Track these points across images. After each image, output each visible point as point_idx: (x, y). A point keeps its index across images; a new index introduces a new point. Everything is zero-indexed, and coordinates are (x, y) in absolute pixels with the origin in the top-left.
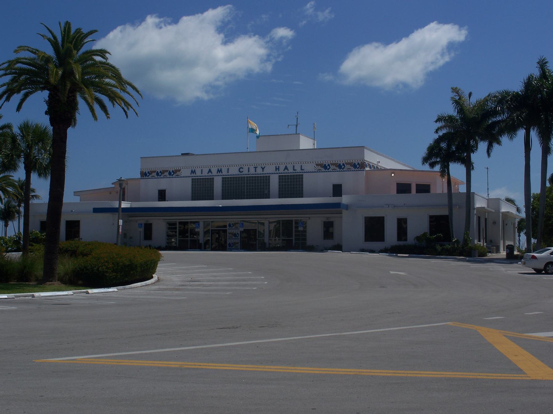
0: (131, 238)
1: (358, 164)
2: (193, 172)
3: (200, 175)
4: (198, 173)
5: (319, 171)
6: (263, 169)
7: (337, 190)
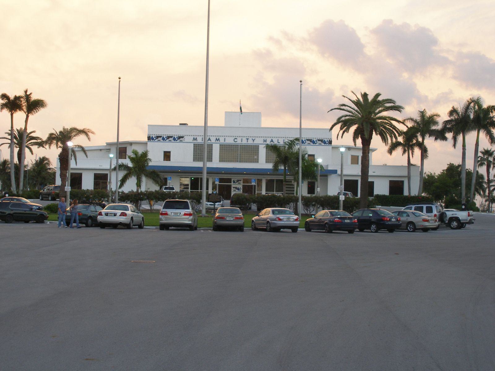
2: (195, 139)
3: (246, 142)
6: (254, 140)
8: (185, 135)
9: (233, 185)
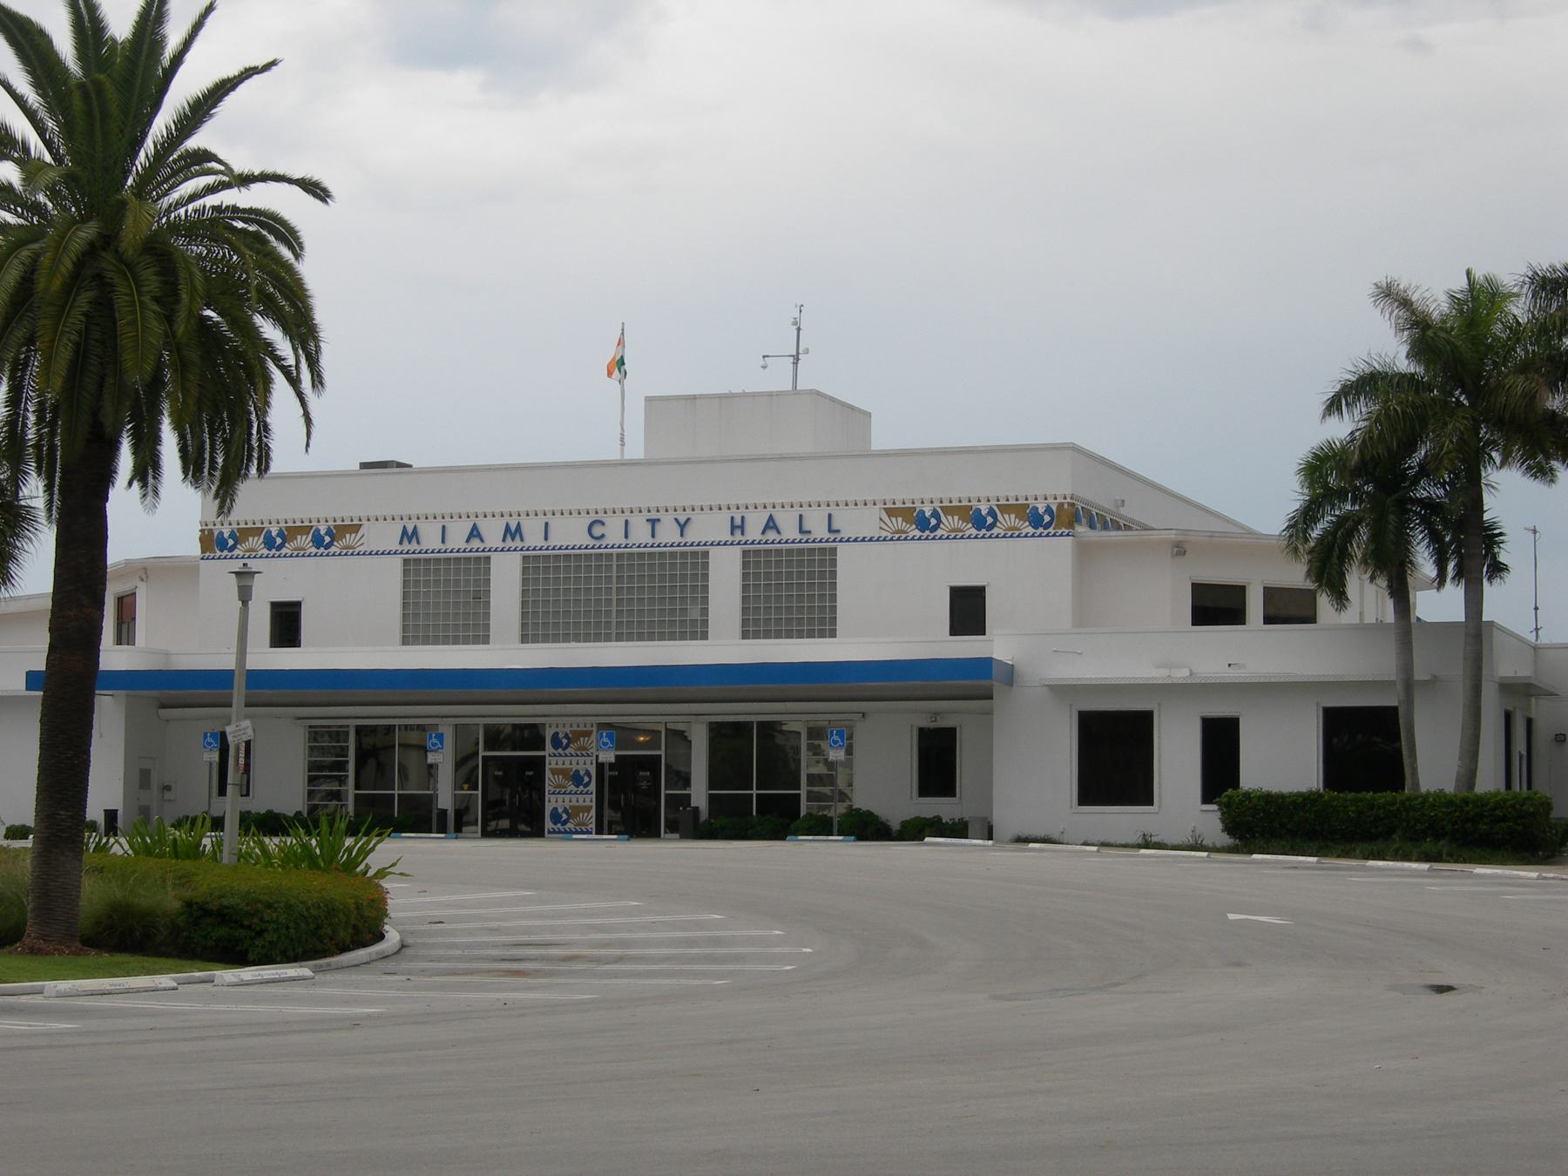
0: (168, 788)
1: (1049, 510)
2: (409, 535)
4: (430, 539)
5: (899, 536)
6: (682, 527)
7: (968, 610)
8: (363, 514)
9: (554, 761)
